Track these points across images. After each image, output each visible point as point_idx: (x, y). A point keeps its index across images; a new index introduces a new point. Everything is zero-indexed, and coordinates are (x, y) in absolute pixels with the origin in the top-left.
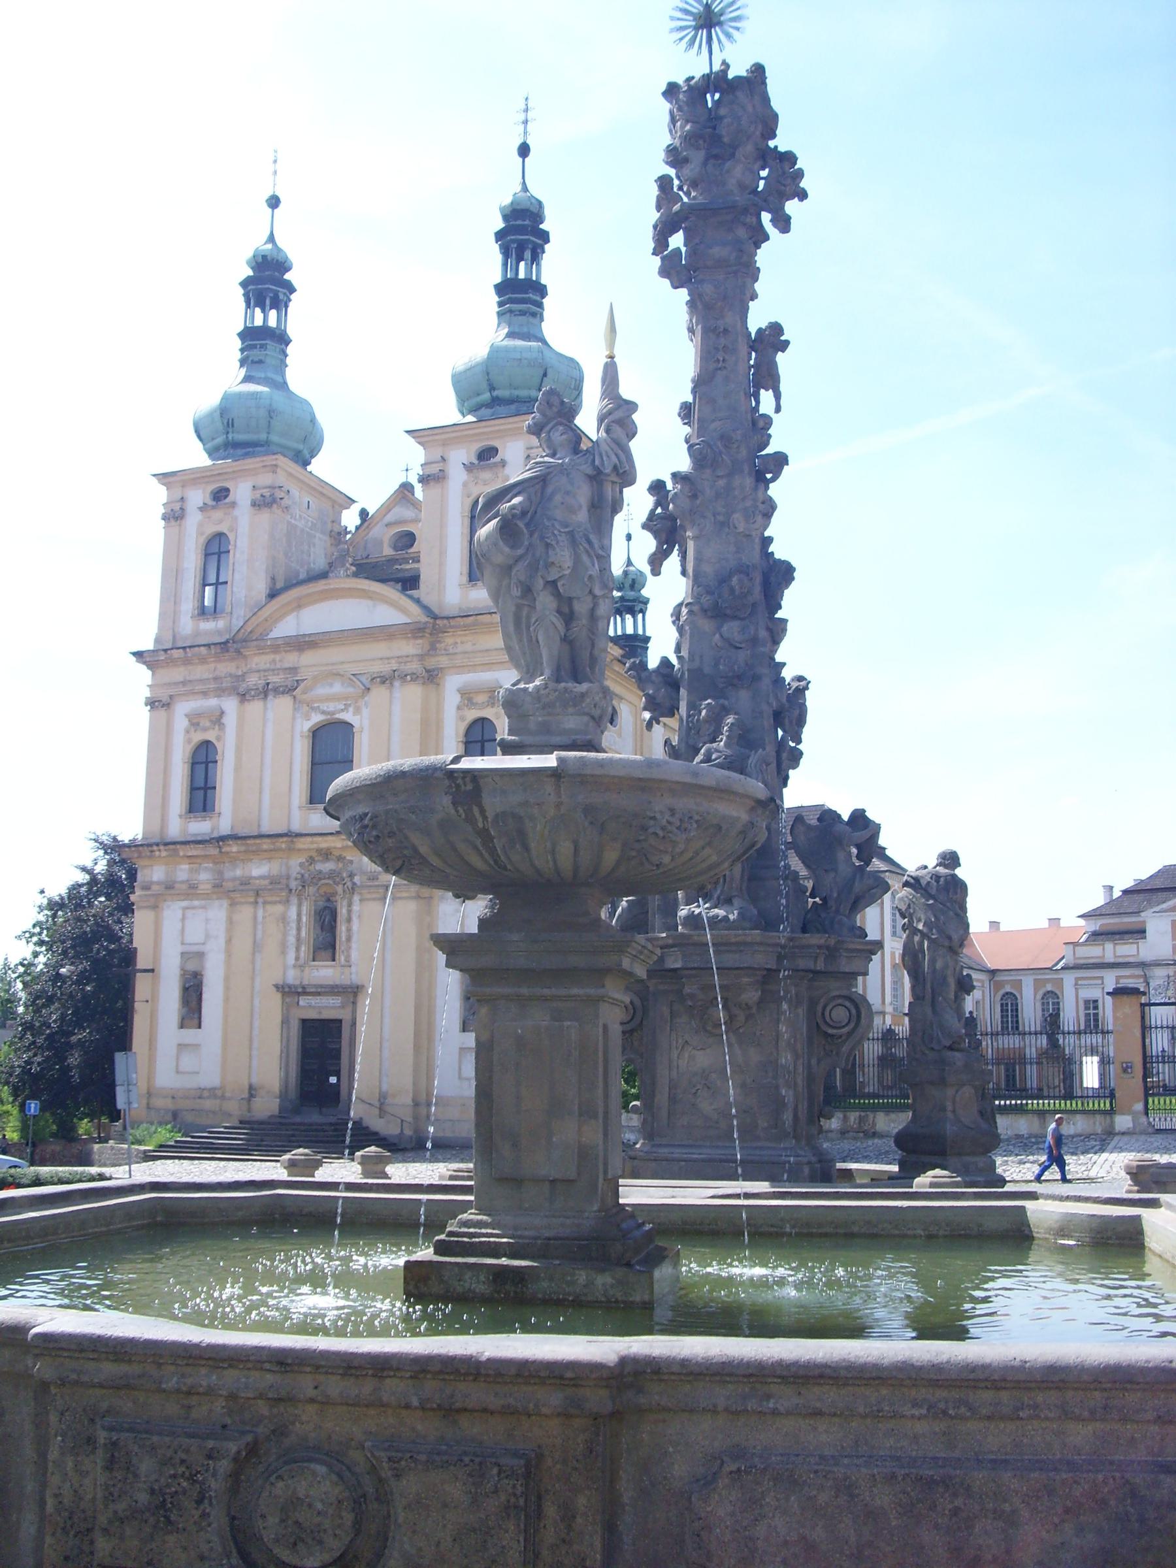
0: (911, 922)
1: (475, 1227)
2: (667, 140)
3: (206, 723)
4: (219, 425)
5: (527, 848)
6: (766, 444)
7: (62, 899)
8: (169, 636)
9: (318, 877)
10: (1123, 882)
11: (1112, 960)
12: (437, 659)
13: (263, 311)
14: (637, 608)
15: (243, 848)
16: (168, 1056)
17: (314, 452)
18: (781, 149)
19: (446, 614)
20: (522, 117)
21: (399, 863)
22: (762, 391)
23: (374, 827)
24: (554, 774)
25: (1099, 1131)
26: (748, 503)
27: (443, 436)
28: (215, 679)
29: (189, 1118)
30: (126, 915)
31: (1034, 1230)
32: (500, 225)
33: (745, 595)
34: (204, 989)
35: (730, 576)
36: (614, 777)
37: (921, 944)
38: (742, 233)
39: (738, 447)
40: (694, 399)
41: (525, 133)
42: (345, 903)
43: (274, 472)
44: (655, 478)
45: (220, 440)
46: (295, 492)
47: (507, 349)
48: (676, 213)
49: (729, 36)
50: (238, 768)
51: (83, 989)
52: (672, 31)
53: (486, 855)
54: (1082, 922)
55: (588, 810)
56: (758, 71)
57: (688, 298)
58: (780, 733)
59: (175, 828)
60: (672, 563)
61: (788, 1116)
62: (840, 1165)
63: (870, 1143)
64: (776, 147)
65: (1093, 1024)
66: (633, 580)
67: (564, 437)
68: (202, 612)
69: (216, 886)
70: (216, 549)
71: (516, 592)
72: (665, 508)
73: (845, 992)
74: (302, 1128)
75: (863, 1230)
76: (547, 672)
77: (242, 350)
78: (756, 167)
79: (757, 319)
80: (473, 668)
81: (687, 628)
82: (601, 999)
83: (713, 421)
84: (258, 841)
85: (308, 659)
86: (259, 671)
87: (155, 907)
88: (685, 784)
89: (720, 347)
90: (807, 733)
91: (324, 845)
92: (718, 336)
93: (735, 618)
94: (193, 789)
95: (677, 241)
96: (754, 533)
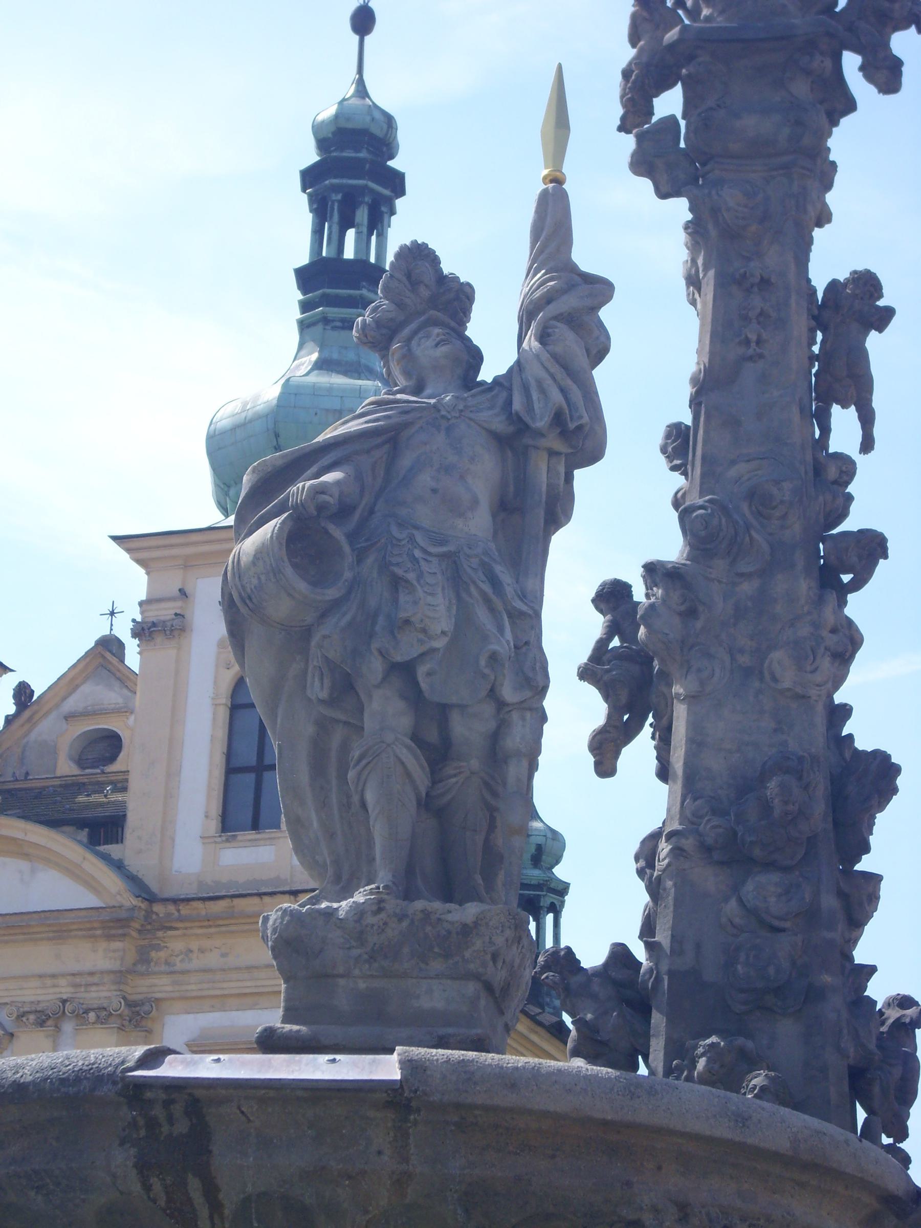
6: (843, 514)
14: (546, 902)
22: (836, 409)
32: (312, 157)
35: (763, 777)
36: (545, 1114)
38: (801, 88)
39: (784, 517)
40: (696, 418)
44: (609, 576)
47: (315, 391)
48: (672, 46)
57: (689, 216)
58: (861, 1115)
60: (641, 751)
67: (443, 349)
71: (318, 689)
72: (628, 636)
76: (384, 877)
79: (829, 261)
80: (221, 1002)
81: (669, 884)
83: (733, 463)
88: (711, 1141)
89: (752, 314)
92: (748, 291)
93: (769, 866)
95: (670, 103)
96: (813, 692)
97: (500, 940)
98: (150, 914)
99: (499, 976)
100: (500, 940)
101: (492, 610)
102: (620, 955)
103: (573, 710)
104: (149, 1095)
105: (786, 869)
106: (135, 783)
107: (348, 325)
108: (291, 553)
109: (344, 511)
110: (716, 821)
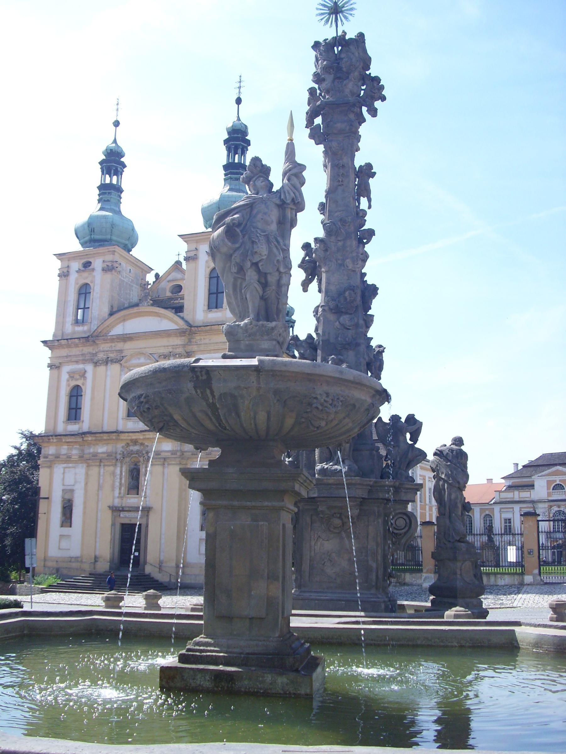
0: (438, 474)
1: (203, 646)
2: (314, 70)
3: (77, 376)
4: (87, 231)
5: (238, 415)
6: (364, 225)
7: (5, 462)
8: (60, 333)
9: (131, 453)
10: (523, 462)
11: (518, 500)
12: (191, 347)
13: (110, 177)
15: (94, 438)
16: (54, 540)
17: (133, 245)
18: (372, 75)
19: (196, 325)
20: (238, 85)
21: (161, 425)
22: (362, 198)
23: (147, 402)
24: (256, 369)
25: (516, 583)
26: (354, 254)
27: (197, 238)
28: (82, 355)
29: (65, 572)
30: (36, 470)
31: (520, 643)
32: (226, 136)
33: (351, 303)
34: (74, 508)
35: (344, 292)
36: (293, 372)
37: (444, 485)
38: (352, 116)
39: (349, 225)
40: (327, 201)
41: (239, 92)
42: (144, 466)
43: (114, 254)
44: (306, 241)
45: (87, 238)
46: (123, 264)
47: (229, 197)
48: (318, 106)
49: (346, 18)
50: (93, 399)
51: (14, 507)
52: (317, 15)
53: (214, 419)
54: (503, 481)
55: (277, 392)
56: (361, 36)
59: (61, 428)
60: (314, 285)
61: (374, 577)
62: (399, 602)
63: (403, 588)
64: (370, 74)
65: (508, 530)
66: (288, 312)
67: (264, 183)
68: (77, 322)
69: (80, 457)
70: (84, 291)
71: (234, 270)
73: (404, 511)
74: (121, 577)
75: (424, 643)
76: (252, 316)
77: (99, 195)
78: (360, 84)
79: (359, 161)
81: (322, 318)
82: (282, 508)
83: (336, 212)
84: (102, 435)
85: (128, 346)
86: (104, 351)
87: (50, 467)
90: (383, 374)
91: (134, 438)
92: (339, 168)
93: (346, 313)
94: (70, 409)
95: (318, 121)
96: (357, 270)
97: (281, 331)
98: (191, 330)
99: (281, 340)
100: (281, 331)
101: (277, 248)
102: (310, 336)
103: (298, 275)
104: (196, 370)
105: (351, 314)
106: (186, 297)
107: (238, 179)
108: (226, 236)
109: (239, 225)
110: (333, 303)
